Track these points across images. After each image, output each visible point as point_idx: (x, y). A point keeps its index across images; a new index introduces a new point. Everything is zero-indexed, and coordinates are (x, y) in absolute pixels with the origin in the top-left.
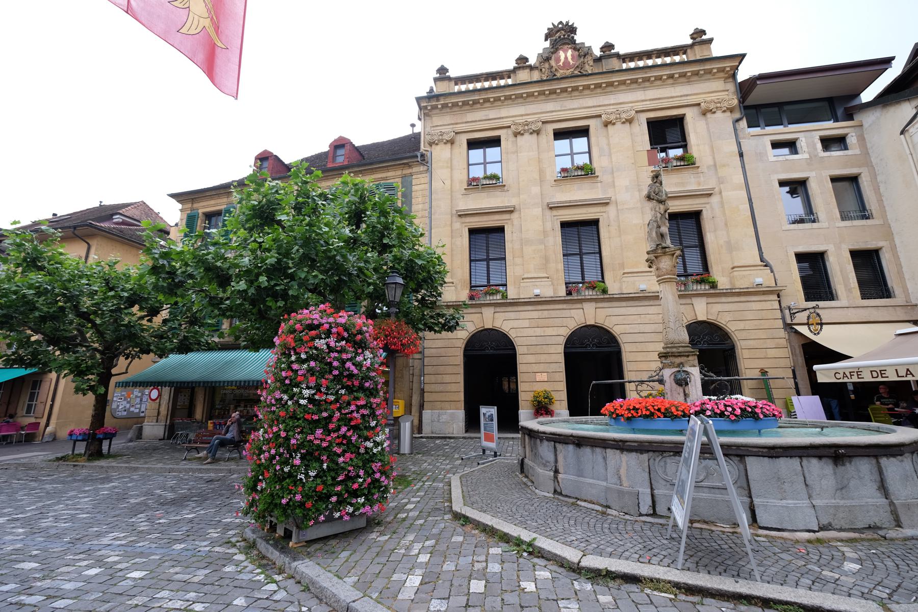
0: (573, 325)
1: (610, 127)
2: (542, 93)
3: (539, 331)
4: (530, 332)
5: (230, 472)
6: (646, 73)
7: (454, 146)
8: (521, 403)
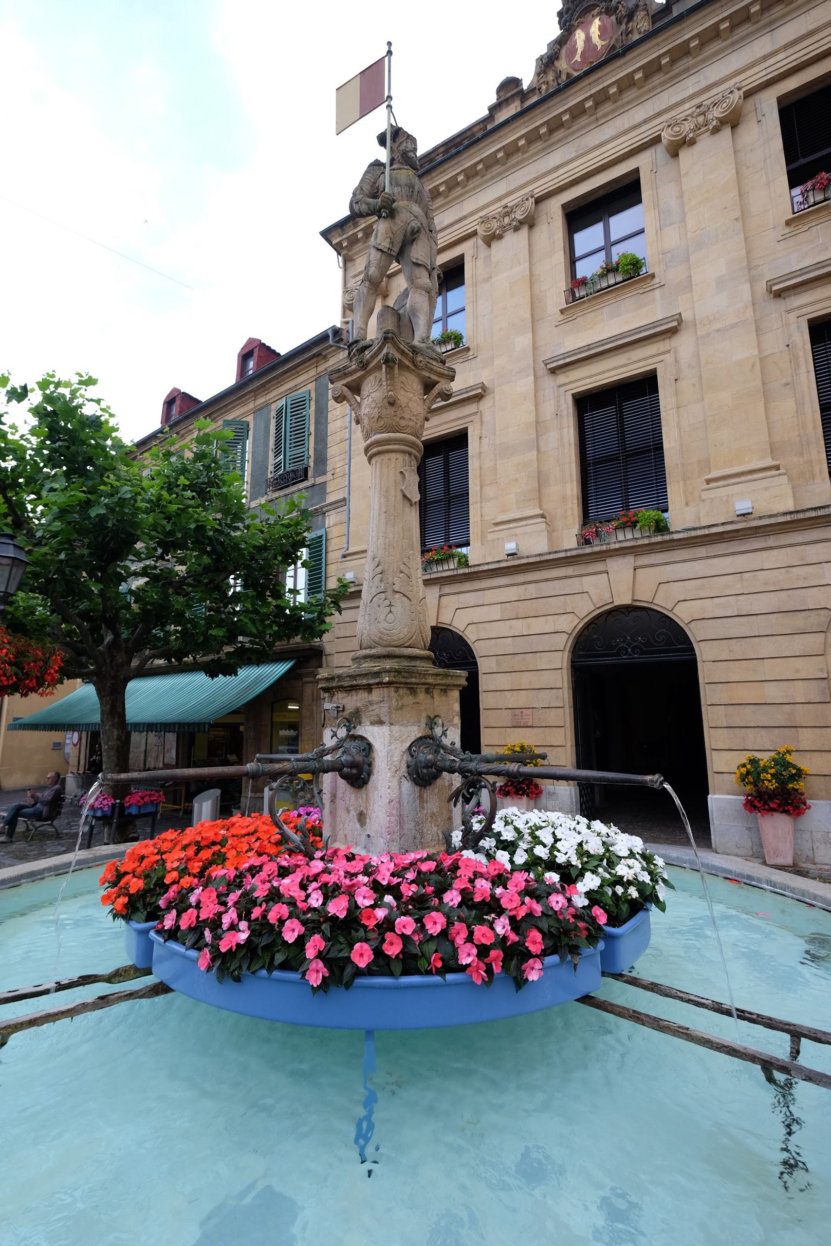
0: (585, 609)
2: (533, 137)
3: (519, 627)
4: (503, 629)
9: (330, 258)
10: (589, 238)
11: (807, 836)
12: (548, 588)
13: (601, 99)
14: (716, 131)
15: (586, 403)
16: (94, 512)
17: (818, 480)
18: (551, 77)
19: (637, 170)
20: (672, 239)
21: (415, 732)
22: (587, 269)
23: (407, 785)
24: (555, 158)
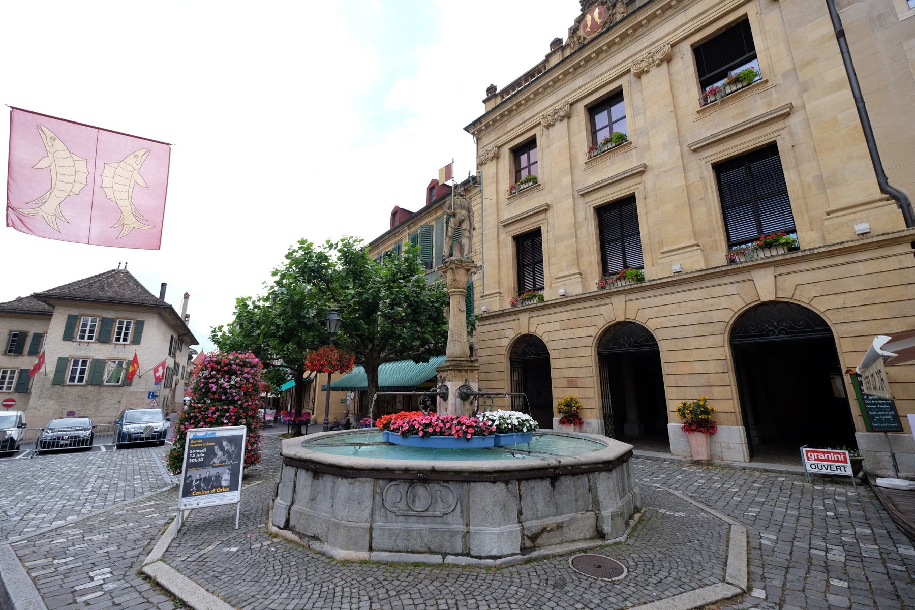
0: (602, 323)
1: (643, 77)
2: (566, 74)
3: (569, 334)
4: (561, 335)
5: (145, 413)
7: (500, 159)
8: (670, 416)
9: (470, 138)
10: (601, 119)
11: (718, 445)
12: (583, 313)
13: (599, 52)
14: (659, 65)
15: (601, 211)
16: (365, 296)
17: (720, 250)
18: (576, 39)
19: (621, 86)
20: (640, 122)
21: (461, 384)
22: (602, 136)
23: (458, 400)
24: (579, 82)
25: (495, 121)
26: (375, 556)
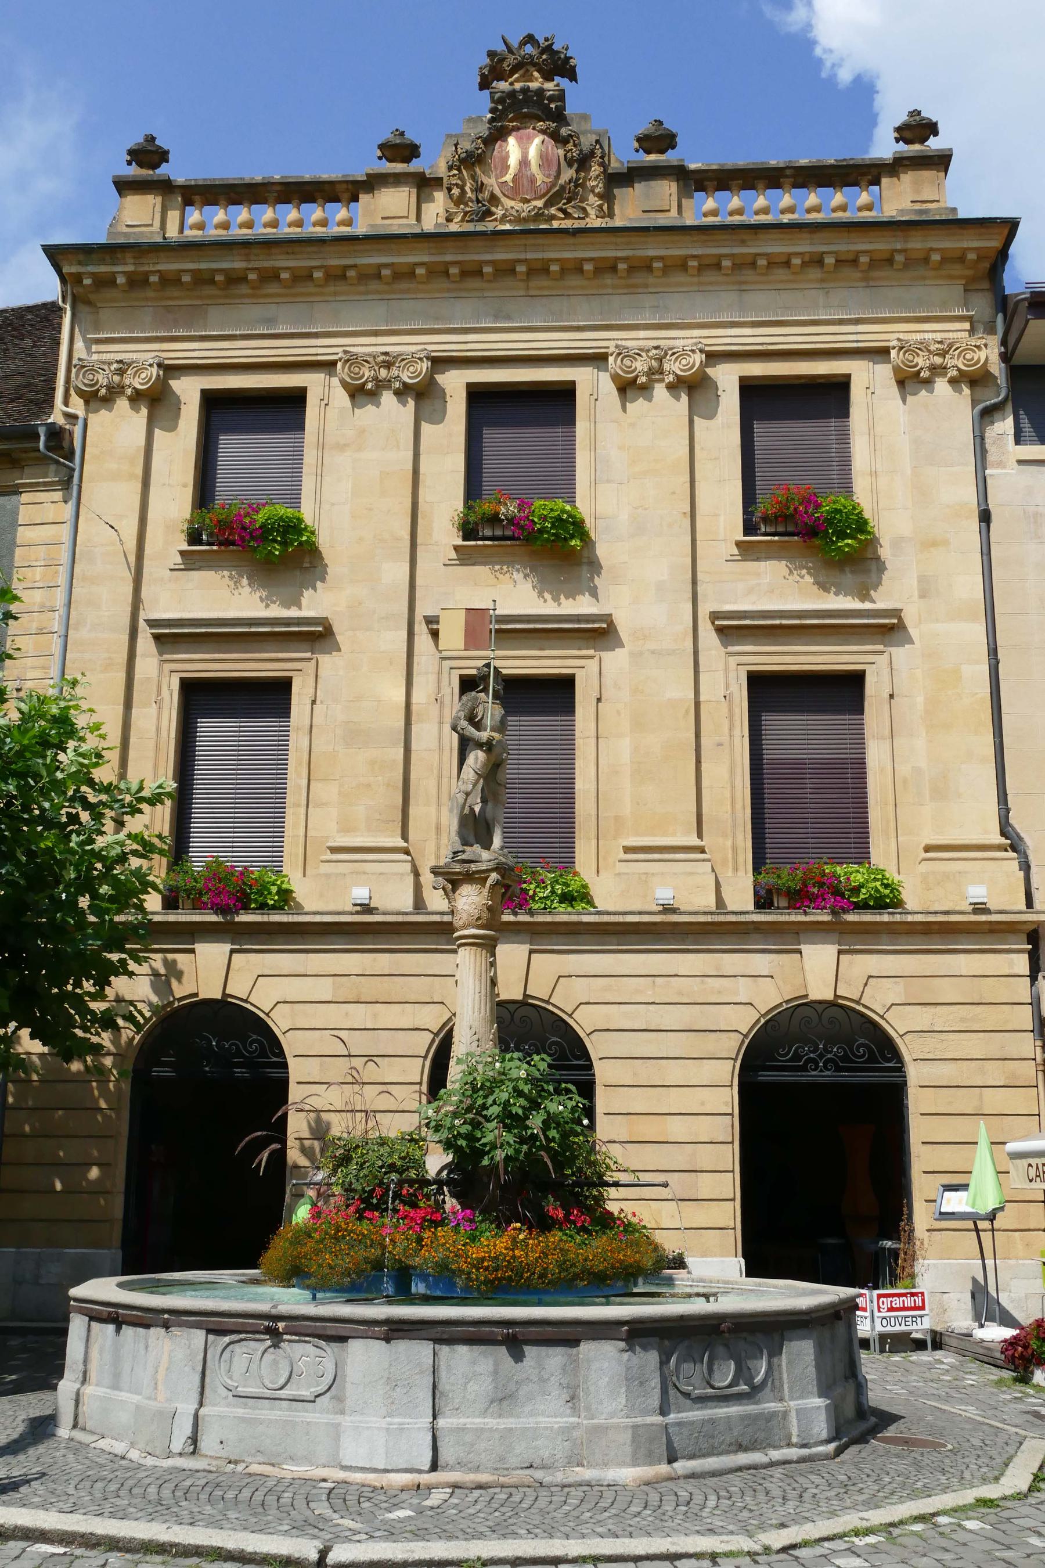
4: (332, 1016)
6: (743, 242)
17: (741, 873)
25: (169, 281)
26: (682, 1466)
